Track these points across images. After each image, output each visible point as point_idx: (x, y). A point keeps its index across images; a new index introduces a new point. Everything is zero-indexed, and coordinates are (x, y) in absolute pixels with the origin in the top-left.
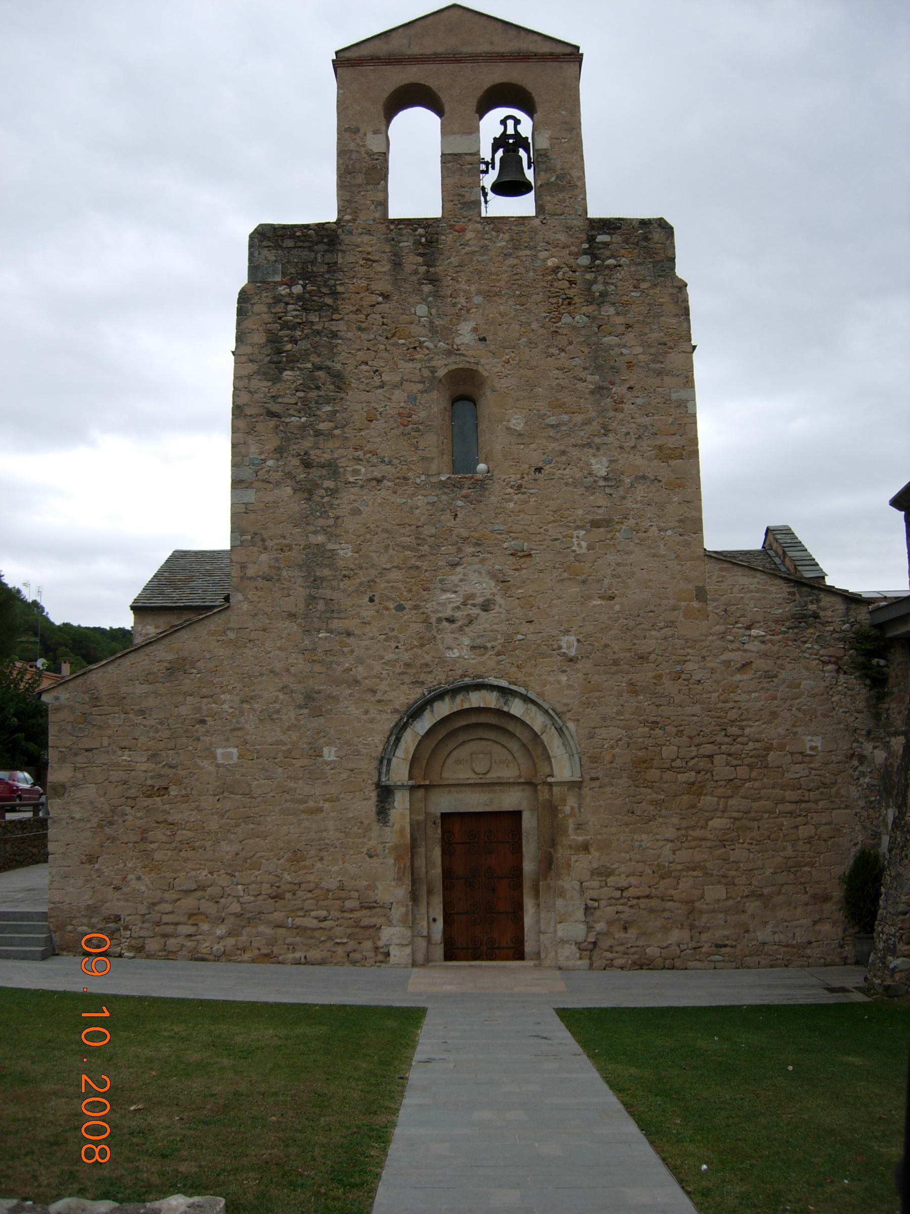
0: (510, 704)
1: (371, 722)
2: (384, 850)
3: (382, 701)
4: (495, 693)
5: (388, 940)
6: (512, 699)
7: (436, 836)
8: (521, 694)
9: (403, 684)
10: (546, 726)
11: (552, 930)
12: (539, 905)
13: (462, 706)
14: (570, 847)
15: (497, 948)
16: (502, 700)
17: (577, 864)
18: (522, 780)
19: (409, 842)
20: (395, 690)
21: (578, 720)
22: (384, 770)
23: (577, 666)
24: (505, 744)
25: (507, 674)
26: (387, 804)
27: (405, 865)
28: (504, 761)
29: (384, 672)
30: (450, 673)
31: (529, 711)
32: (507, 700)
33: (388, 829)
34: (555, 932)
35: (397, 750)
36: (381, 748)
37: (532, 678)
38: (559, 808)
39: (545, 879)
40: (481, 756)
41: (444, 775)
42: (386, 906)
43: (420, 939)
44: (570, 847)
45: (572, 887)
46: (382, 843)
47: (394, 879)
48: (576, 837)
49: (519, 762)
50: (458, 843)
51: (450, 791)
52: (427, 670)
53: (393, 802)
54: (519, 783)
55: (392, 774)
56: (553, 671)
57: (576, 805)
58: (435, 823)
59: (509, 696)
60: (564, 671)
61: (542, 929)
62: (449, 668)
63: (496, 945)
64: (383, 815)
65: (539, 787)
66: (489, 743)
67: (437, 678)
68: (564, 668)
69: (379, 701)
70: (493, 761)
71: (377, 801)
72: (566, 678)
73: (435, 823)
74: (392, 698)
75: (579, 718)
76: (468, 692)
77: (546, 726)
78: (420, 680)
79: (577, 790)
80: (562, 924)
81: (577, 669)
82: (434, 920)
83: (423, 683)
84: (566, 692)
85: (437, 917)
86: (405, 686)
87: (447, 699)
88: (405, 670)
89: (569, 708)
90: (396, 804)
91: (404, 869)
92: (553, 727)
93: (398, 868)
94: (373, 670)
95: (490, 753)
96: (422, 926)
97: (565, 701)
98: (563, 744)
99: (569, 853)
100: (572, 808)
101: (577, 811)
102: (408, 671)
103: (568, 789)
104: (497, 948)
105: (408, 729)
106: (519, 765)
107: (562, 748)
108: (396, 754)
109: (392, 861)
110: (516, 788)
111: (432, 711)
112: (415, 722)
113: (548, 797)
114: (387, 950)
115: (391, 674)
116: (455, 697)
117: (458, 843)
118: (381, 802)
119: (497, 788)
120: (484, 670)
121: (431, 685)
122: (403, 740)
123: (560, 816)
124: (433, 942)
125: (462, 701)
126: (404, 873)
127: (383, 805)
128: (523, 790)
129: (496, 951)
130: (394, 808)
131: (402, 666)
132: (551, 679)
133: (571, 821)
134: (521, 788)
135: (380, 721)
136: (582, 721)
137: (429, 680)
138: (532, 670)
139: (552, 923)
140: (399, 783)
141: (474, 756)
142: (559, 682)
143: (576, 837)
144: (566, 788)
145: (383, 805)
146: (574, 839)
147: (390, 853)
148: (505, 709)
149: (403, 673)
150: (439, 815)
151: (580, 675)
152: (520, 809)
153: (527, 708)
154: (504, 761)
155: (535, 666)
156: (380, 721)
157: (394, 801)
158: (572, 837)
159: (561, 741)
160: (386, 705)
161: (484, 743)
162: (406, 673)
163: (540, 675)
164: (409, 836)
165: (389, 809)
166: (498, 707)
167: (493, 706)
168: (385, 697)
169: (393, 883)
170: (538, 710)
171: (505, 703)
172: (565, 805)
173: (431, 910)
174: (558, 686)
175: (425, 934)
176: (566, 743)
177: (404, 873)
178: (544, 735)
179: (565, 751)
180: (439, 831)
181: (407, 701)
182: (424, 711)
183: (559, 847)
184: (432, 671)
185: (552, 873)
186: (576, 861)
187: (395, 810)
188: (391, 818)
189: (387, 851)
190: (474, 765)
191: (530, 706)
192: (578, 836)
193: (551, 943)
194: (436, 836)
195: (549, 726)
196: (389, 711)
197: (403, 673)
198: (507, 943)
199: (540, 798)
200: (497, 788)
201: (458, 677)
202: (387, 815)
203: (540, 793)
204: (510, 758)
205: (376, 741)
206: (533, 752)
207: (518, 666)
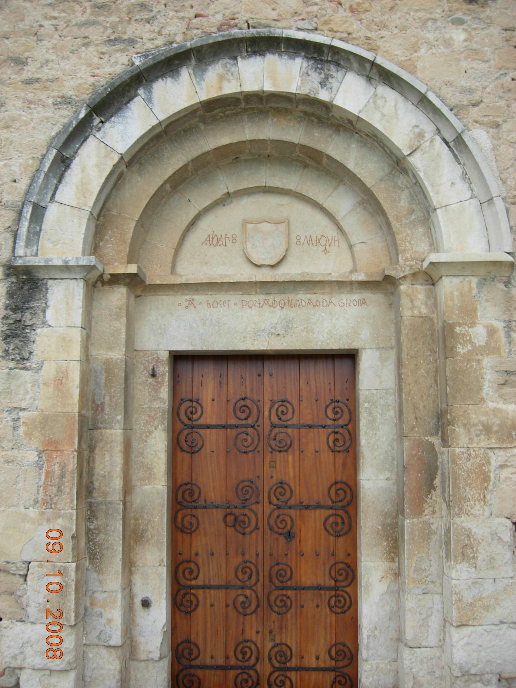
0: (335, 85)
1: (7, 127)
2: (15, 428)
3: (37, 80)
4: (299, 61)
5: (15, 657)
6: (340, 75)
7: (156, 405)
8: (361, 59)
9: (86, 45)
10: (421, 135)
11: (432, 640)
12: (398, 574)
13: (220, 88)
14: (487, 429)
15: (297, 669)
16: (315, 77)
17: (505, 473)
18: (361, 277)
19: (75, 408)
20: (68, 58)
21: (498, 126)
22: (24, 230)
23: (488, 12)
24: (320, 199)
25: (326, 23)
26: (27, 315)
27: (63, 467)
28: (318, 241)
29: (47, 24)
30: (195, 21)
31: (380, 102)
32: (327, 78)
33: (27, 375)
34: (442, 644)
35: (61, 187)
36: (23, 185)
37: (384, 33)
38: (458, 329)
39: (418, 511)
40: (265, 227)
41: (179, 270)
42: (13, 569)
43: (104, 652)
44: (487, 429)
45: (494, 534)
46: (11, 410)
47: (36, 502)
48: (501, 405)
49: (354, 239)
50: (208, 427)
51: (191, 302)
52: (145, 15)
53: (44, 311)
54: (351, 283)
55: (44, 242)
56: (435, 20)
57: (499, 325)
58: (153, 375)
59: (333, 68)
60: (459, 22)
61: (409, 635)
62: (191, 13)
63: (293, 663)
64: (17, 341)
65: (402, 288)
66: (285, 200)
67: (165, 32)
68: (459, 15)
69: (29, 82)
70: (293, 236)
71: (7, 307)
72: (463, 36)
73: (153, 375)
74: (59, 74)
75: (499, 120)
76: (235, 58)
77: (421, 135)
78: (125, 37)
79: (501, 286)
80: (465, 631)
81: (488, 17)
82: (146, 604)
83: (131, 42)
84: (464, 64)
85: (153, 598)
86: (91, 49)
87: (185, 73)
88: (92, 18)
89: (476, 97)
90: (49, 313)
91: (62, 476)
92: (438, 139)
93: (48, 474)
94: (22, 20)
95: (288, 223)
96: (110, 621)
97: (463, 83)
98: (465, 176)
99: (483, 444)
100: (491, 332)
101: (504, 340)
102: (102, 18)
103: (481, 284)
104: (297, 669)
105: (91, 139)
106: (351, 247)
107: (462, 187)
108: (57, 197)
109: (32, 457)
110: (345, 297)
111: (149, 100)
112: (107, 125)
113: (424, 311)
114: (12, 681)
115: (62, 24)
116: (204, 71)
117: (208, 427)
118: (15, 309)
119: (302, 296)
120: (274, 15)
121: (149, 45)
122: (76, 165)
123: (461, 350)
124: (143, 656)
125: (221, 78)
126: (60, 490)
127: (18, 316)
128: (363, 302)
129: (293, 675)
130: (44, 323)
131: (89, 10)
132: (430, 36)
133: (487, 362)
134: (356, 297)
135: (27, 124)
136: (505, 127)
137: (146, 36)
138: (386, 17)
139: (435, 622)
140: (58, 262)
141: (249, 226)
142: (448, 43)
143: (501, 405)
144: (474, 281)
145: (18, 316)
146: (496, 411)
147: (28, 435)
148: (324, 96)
149: (88, 24)
150: (165, 356)
151: (495, 30)
152: (355, 345)
153: (375, 95)
154: (318, 241)
155: (392, 9)
156: (27, 124)
157: (47, 307)
158: (491, 405)
159: (458, 170)
160: (46, 88)
161: (273, 200)
162: (94, 23)
163: (403, 29)
164: (76, 393)
165: (32, 327)
166: (304, 91)
167: (293, 89)
168: (45, 73)
169: (33, 513)
170: (400, 99)
171: (323, 84)
172: (473, 324)
173: (137, 580)
174: (446, 51)
175: (116, 639)
176: (472, 174)
177: (60, 490)
178: (417, 155)
179: (469, 194)
180: (165, 393)
181: (92, 80)
182: (131, 99)
183: (459, 430)
184: (153, 18)
185: (436, 496)
186: (502, 466)
187: (46, 330)
188: (34, 347)
189: (22, 429)
190: (249, 245)
191: (383, 90)
192: (506, 401)
193: (431, 673)
194: (156, 405)
195: (428, 136)
196: (50, 101)
197: (88, 24)
198: (317, 658)
199: (407, 313)
200: (300, 296)
201: (214, 30)
202: (26, 341)
203: (405, 302)
204: (331, 232)
205: (16, 169)
206: (385, 206)
207: (352, 10)
